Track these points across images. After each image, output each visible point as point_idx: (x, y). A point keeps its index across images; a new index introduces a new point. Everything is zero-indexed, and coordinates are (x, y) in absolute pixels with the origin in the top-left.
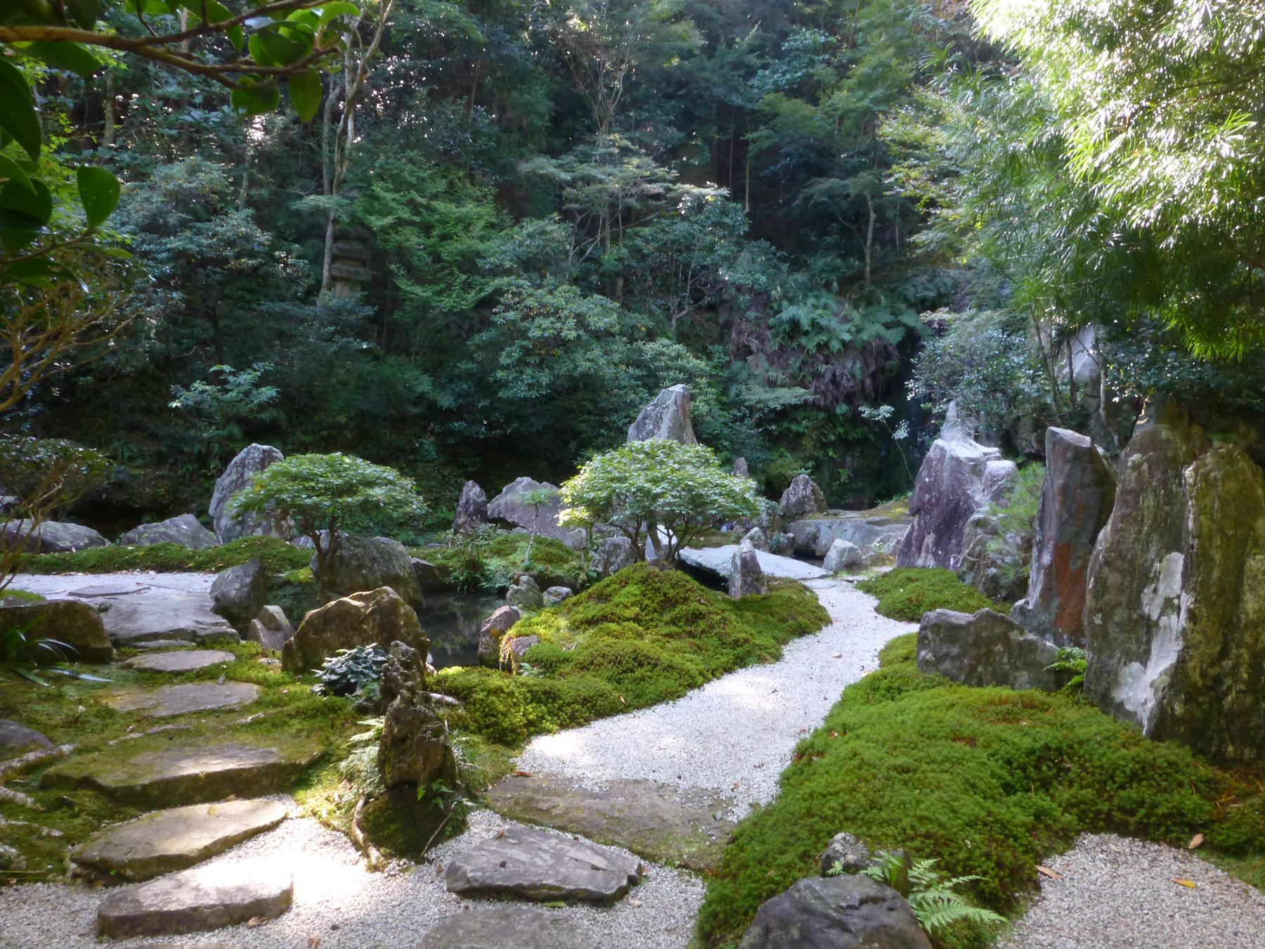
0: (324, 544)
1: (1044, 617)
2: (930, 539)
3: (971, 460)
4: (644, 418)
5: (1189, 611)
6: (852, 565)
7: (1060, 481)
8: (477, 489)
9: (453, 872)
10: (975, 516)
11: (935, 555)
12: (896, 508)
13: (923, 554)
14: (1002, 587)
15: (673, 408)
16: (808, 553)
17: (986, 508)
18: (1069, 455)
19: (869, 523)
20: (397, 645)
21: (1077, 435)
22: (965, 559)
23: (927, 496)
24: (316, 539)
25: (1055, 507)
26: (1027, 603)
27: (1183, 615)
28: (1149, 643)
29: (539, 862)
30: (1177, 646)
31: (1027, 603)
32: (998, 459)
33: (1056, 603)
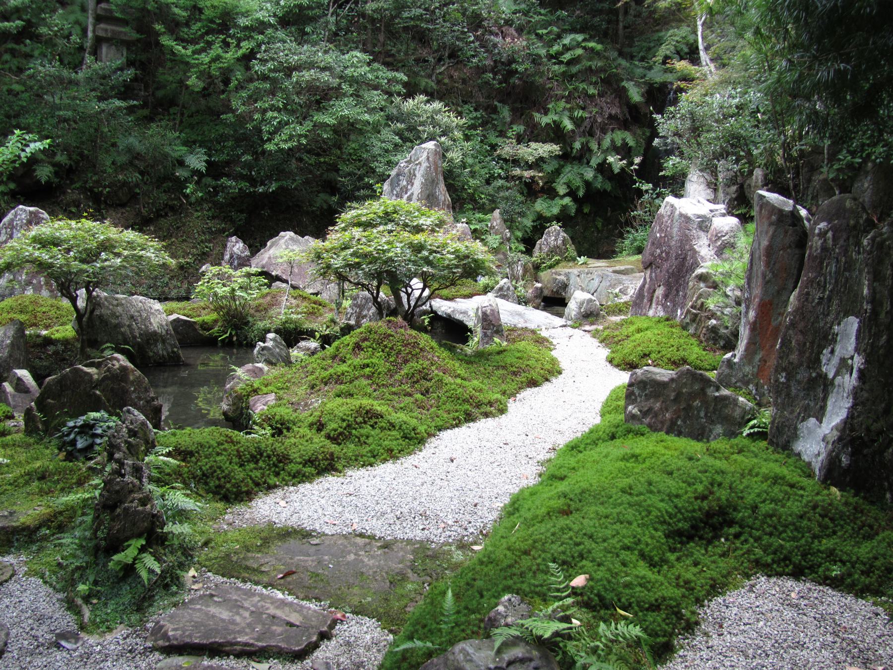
0: (81, 303)
1: (747, 369)
2: (660, 292)
3: (699, 217)
4: (398, 175)
5: (860, 371)
6: (589, 316)
7: (765, 243)
8: (241, 245)
9: (158, 630)
10: (699, 271)
11: (664, 306)
12: (628, 261)
13: (654, 305)
14: (720, 337)
15: (425, 165)
16: (554, 302)
17: (709, 264)
18: (774, 218)
19: (615, 272)
20: (129, 411)
21: (781, 198)
22: (688, 312)
23: (658, 251)
24: (74, 300)
25: (761, 267)
26: (734, 356)
27: (855, 375)
28: (825, 399)
29: (238, 619)
30: (847, 403)
31: (734, 356)
32: (723, 215)
33: (758, 357)
